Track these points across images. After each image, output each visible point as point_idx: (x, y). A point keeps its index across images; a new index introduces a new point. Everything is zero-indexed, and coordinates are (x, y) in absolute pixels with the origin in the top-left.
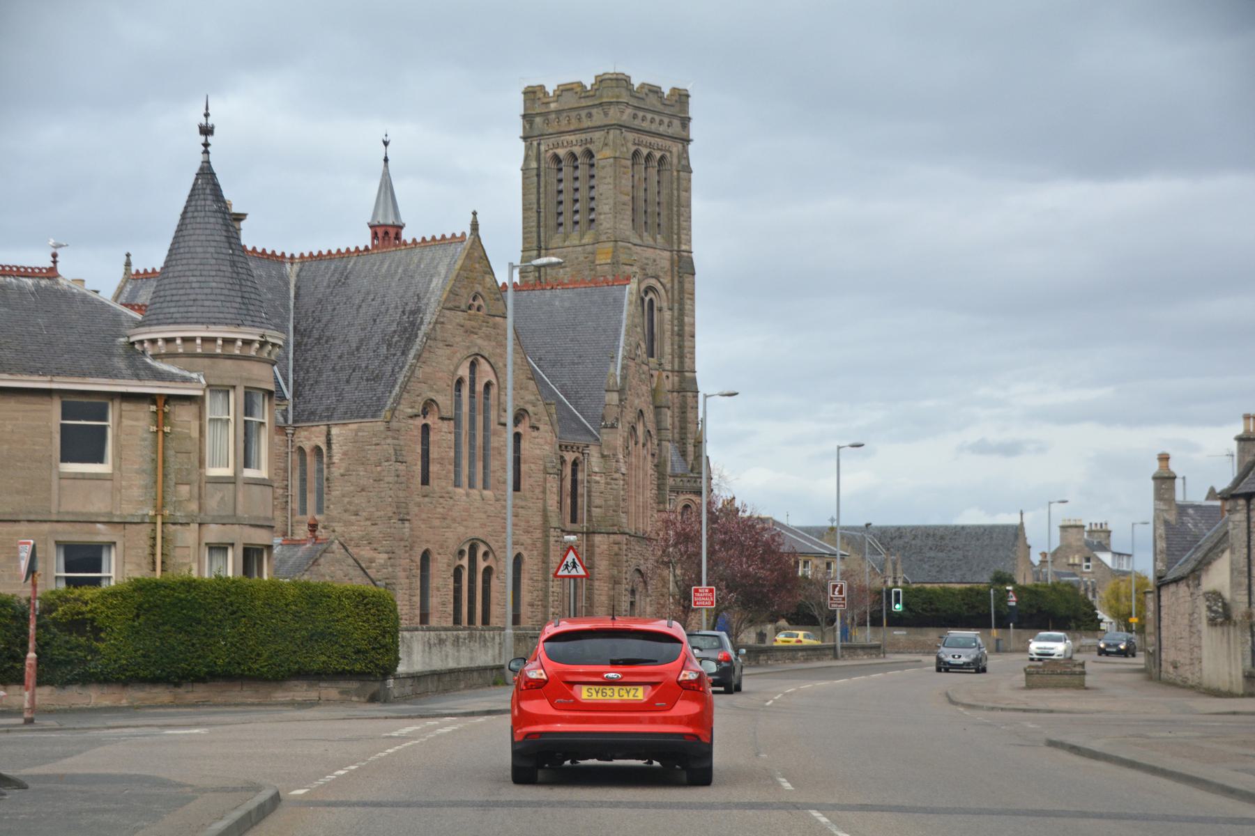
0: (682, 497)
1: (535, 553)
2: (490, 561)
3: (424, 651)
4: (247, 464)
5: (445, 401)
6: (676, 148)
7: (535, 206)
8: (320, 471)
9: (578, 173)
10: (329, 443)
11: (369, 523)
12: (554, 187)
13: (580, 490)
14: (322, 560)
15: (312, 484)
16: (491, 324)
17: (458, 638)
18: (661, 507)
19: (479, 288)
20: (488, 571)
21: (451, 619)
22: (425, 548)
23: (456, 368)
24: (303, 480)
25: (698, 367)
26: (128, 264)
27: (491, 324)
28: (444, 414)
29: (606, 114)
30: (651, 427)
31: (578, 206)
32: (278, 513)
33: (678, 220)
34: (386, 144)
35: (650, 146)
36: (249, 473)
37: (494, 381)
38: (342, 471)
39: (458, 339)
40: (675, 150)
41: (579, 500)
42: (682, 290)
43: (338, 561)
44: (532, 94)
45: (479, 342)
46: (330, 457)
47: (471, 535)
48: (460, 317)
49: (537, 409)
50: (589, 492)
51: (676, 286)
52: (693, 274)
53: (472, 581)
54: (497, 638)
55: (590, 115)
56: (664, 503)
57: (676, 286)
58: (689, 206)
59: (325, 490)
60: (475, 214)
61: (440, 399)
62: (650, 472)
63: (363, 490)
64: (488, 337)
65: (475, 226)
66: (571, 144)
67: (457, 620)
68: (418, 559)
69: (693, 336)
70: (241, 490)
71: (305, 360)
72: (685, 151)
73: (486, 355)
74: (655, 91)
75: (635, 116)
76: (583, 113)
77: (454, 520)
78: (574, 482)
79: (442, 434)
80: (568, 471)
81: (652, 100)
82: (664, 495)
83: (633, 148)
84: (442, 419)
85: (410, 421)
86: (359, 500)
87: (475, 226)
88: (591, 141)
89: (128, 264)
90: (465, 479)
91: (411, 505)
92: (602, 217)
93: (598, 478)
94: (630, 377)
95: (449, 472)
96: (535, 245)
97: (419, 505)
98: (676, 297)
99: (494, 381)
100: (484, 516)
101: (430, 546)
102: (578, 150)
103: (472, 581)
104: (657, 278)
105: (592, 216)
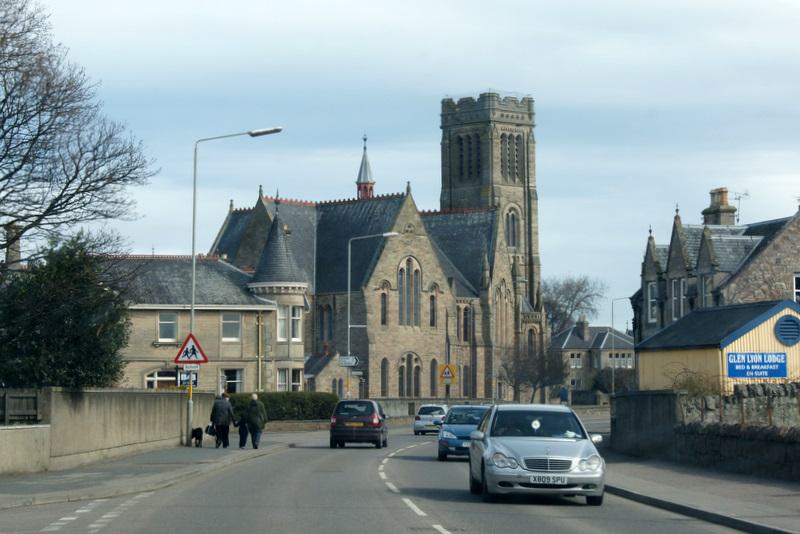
0: (528, 325)
2: (419, 364)
4: (294, 336)
5: (393, 281)
10: (334, 304)
19: (411, 221)
21: (398, 393)
25: (540, 251)
26: (231, 205)
34: (365, 140)
35: (511, 130)
36: (294, 340)
44: (447, 105)
45: (412, 249)
49: (443, 284)
53: (409, 373)
64: (416, 246)
65: (408, 189)
66: (467, 131)
67: (401, 394)
70: (292, 346)
75: (502, 116)
77: (398, 342)
79: (394, 298)
80: (462, 314)
83: (501, 133)
87: (408, 189)
89: (231, 205)
90: (405, 320)
97: (379, 335)
103: (409, 373)
104: (515, 202)
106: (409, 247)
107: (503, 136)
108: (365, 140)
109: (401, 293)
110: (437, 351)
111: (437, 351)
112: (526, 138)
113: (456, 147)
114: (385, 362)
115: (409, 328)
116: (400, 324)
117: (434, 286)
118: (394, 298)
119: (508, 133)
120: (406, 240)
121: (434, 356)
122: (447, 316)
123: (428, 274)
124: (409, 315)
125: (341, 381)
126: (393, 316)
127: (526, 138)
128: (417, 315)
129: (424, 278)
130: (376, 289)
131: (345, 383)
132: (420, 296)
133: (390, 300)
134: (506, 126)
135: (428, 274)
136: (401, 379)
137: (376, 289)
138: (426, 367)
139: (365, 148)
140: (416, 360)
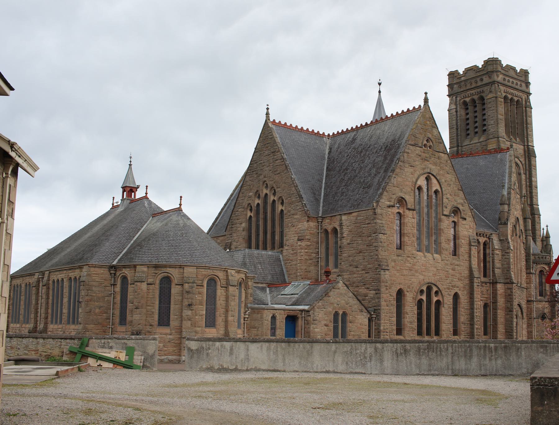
0: (539, 266)
1: (465, 292)
3: (393, 359)
5: (409, 199)
6: (524, 97)
7: (455, 126)
8: (336, 243)
9: (477, 109)
10: (341, 225)
11: (363, 272)
12: (464, 117)
13: (488, 259)
14: (331, 294)
15: (332, 250)
16: (437, 156)
17: (419, 348)
18: (528, 271)
20: (438, 303)
22: (399, 288)
23: (417, 180)
24: (327, 249)
27: (437, 156)
28: (409, 207)
29: (490, 77)
30: (522, 227)
31: (477, 125)
32: (312, 268)
33: (527, 131)
34: (380, 84)
35: (512, 94)
37: (439, 190)
38: (348, 242)
39: (417, 163)
40: (524, 98)
41: (488, 264)
42: (530, 165)
43: (341, 294)
44: (452, 75)
46: (342, 234)
47: (427, 281)
48: (418, 150)
49: (465, 209)
50: (493, 260)
51: (527, 163)
52: (536, 157)
54: (450, 349)
55: (482, 80)
56: (530, 269)
57: (527, 163)
58: (531, 124)
59: (339, 253)
60: (426, 93)
61: (407, 198)
62: (523, 252)
63: (360, 252)
64: (435, 164)
65: (426, 100)
68: (395, 294)
69: (537, 188)
71: (331, 183)
72: (528, 98)
73: (435, 174)
74: (514, 69)
76: (478, 79)
77: (416, 271)
78: (485, 255)
79: (411, 219)
80: (482, 247)
81: (512, 73)
82: (529, 266)
83: (504, 94)
84: (409, 209)
85: (390, 210)
86: (359, 258)
87: (426, 100)
88: (483, 92)
91: (389, 261)
92: (490, 126)
93: (497, 252)
94: (512, 199)
95: (413, 242)
96: (455, 145)
98: (527, 168)
99: (439, 190)
100: (435, 270)
101: (402, 287)
102: (476, 97)
105: (485, 128)
106: (426, 163)
107: (505, 98)
108: (380, 84)
109: (419, 214)
110: (460, 284)
111: (460, 284)
112: (524, 103)
113: (462, 112)
114: (400, 294)
115: (428, 255)
116: (419, 251)
117: (456, 211)
118: (411, 219)
119: (510, 97)
120: (424, 155)
121: (456, 290)
122: (470, 245)
123: (448, 196)
124: (430, 237)
125: (344, 314)
126: (410, 241)
127: (524, 103)
128: (437, 242)
129: (445, 200)
130: (389, 207)
131: (349, 318)
132: (440, 220)
133: (406, 220)
134: (508, 90)
135: (448, 196)
136: (420, 314)
137: (389, 207)
138: (448, 301)
139: (380, 92)
140: (436, 293)
